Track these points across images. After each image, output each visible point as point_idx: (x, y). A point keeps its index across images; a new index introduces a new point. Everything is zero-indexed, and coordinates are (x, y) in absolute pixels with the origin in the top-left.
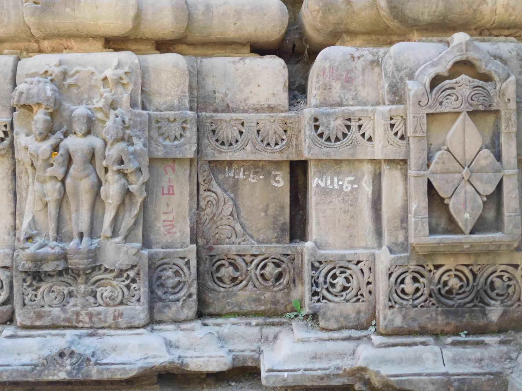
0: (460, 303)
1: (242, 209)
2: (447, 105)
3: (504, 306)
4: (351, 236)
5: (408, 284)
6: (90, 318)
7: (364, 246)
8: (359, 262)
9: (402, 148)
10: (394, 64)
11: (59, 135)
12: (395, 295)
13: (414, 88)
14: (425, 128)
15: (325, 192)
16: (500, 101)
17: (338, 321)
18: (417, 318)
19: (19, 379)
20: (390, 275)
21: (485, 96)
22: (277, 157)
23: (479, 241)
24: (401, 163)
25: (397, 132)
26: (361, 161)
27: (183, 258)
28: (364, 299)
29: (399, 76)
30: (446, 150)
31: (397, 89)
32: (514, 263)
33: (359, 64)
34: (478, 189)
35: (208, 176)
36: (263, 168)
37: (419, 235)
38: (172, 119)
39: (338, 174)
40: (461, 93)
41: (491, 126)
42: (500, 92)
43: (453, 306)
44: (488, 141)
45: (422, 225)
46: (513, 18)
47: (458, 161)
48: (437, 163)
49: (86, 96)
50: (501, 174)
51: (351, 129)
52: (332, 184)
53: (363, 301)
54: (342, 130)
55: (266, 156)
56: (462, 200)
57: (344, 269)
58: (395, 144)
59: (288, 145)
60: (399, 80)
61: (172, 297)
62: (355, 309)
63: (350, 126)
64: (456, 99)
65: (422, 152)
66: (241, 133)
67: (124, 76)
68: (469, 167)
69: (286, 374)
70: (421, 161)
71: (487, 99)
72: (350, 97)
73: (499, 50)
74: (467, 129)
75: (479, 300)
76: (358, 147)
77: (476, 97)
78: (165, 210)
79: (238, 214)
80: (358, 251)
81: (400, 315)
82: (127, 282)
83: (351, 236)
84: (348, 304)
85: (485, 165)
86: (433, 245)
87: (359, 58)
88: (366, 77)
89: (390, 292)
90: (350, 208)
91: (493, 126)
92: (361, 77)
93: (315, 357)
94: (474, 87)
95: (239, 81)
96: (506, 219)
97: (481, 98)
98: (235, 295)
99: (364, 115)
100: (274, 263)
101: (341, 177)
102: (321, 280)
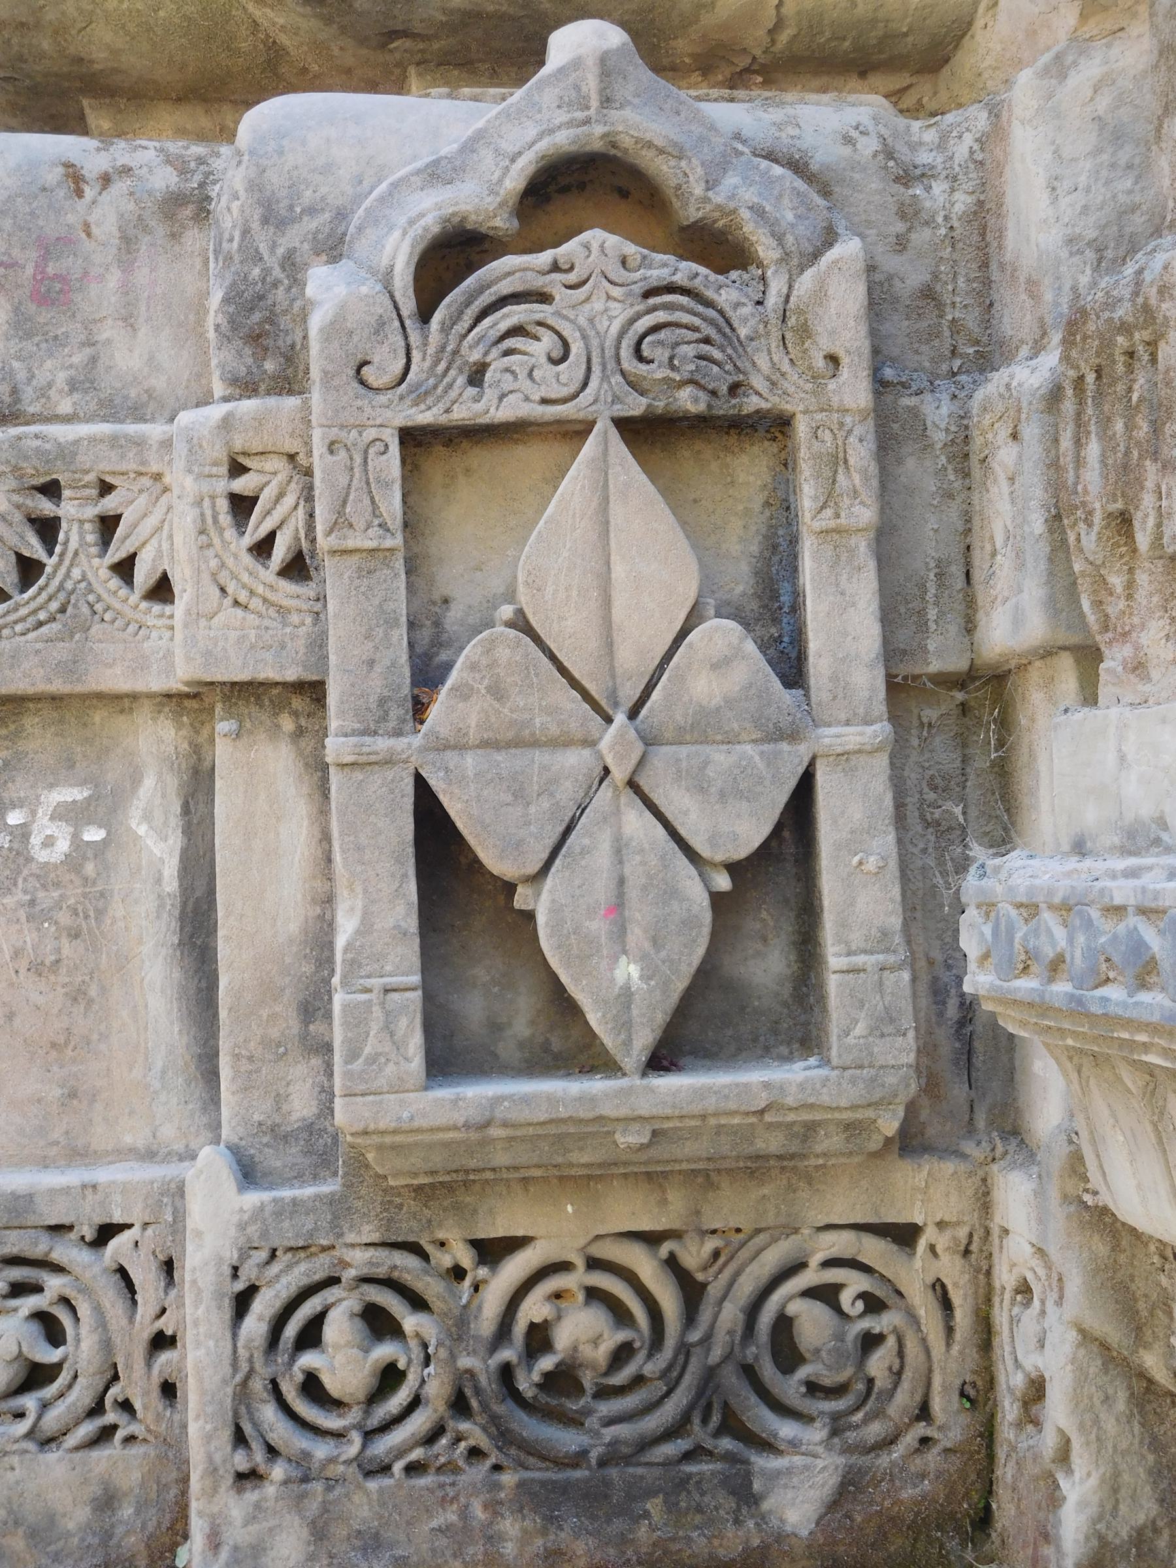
0: (614, 1443)
2: (508, 382)
3: (847, 1450)
4: (73, 1094)
5: (337, 1347)
7: (140, 1144)
8: (106, 1232)
9: (295, 618)
10: (254, 186)
12: (269, 1413)
13: (331, 294)
14: (392, 505)
16: (786, 366)
18: (387, 1534)
20: (242, 1302)
21: (707, 341)
23: (696, 1108)
24: (297, 703)
25: (271, 538)
28: (135, 1428)
29: (280, 251)
30: (510, 624)
31: (271, 320)
33: (107, 212)
34: (683, 832)
40: (582, 321)
41: (757, 505)
42: (784, 319)
43: (578, 1459)
44: (739, 580)
45: (388, 1028)
47: (574, 683)
51: (61, 537)
53: (130, 1439)
54: (13, 540)
56: (602, 890)
58: (255, 603)
60: (277, 273)
62: (85, 1482)
63: (57, 519)
64: (556, 354)
65: (380, 632)
68: (633, 714)
70: (376, 685)
71: (717, 354)
72: (61, 377)
73: (791, 131)
74: (617, 512)
75: (716, 1419)
76: (96, 629)
77: (660, 343)
80: (102, 1175)
81: (297, 1521)
83: (73, 1094)
84: (52, 1456)
85: (717, 701)
86: (451, 1135)
87: (106, 180)
88: (142, 275)
89: (243, 1394)
90: (68, 949)
91: (767, 504)
92: (114, 279)
94: (647, 294)
96: (833, 984)
97: (689, 350)
99: (123, 467)
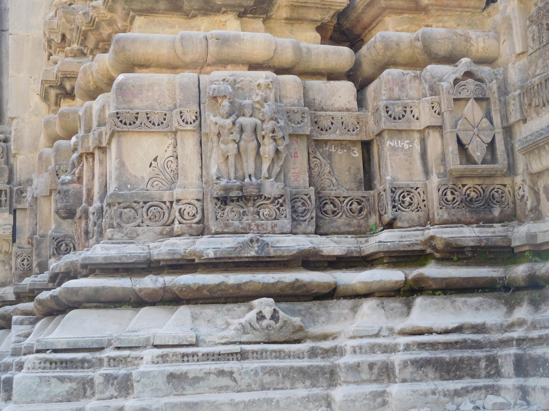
1: (335, 170)
6: (258, 228)
8: (417, 188)
11: (234, 116)
15: (394, 149)
17: (408, 222)
19: (227, 256)
20: (439, 190)
22: (355, 138)
26: (412, 131)
27: (306, 195)
32: (504, 184)
35: (314, 149)
36: (346, 145)
37: (454, 163)
38: (296, 111)
39: (401, 139)
46: (487, 55)
48: (461, 125)
49: (247, 95)
50: (494, 132)
52: (398, 144)
55: (348, 138)
57: (409, 192)
59: (360, 130)
61: (301, 218)
66: (332, 123)
67: (270, 83)
69: (389, 243)
78: (293, 167)
79: (333, 173)
82: (278, 206)
87: (407, 74)
88: (412, 84)
90: (409, 158)
93: (402, 237)
95: (328, 93)
98: (336, 221)
100: (357, 202)
101: (402, 141)
102: (397, 198)
